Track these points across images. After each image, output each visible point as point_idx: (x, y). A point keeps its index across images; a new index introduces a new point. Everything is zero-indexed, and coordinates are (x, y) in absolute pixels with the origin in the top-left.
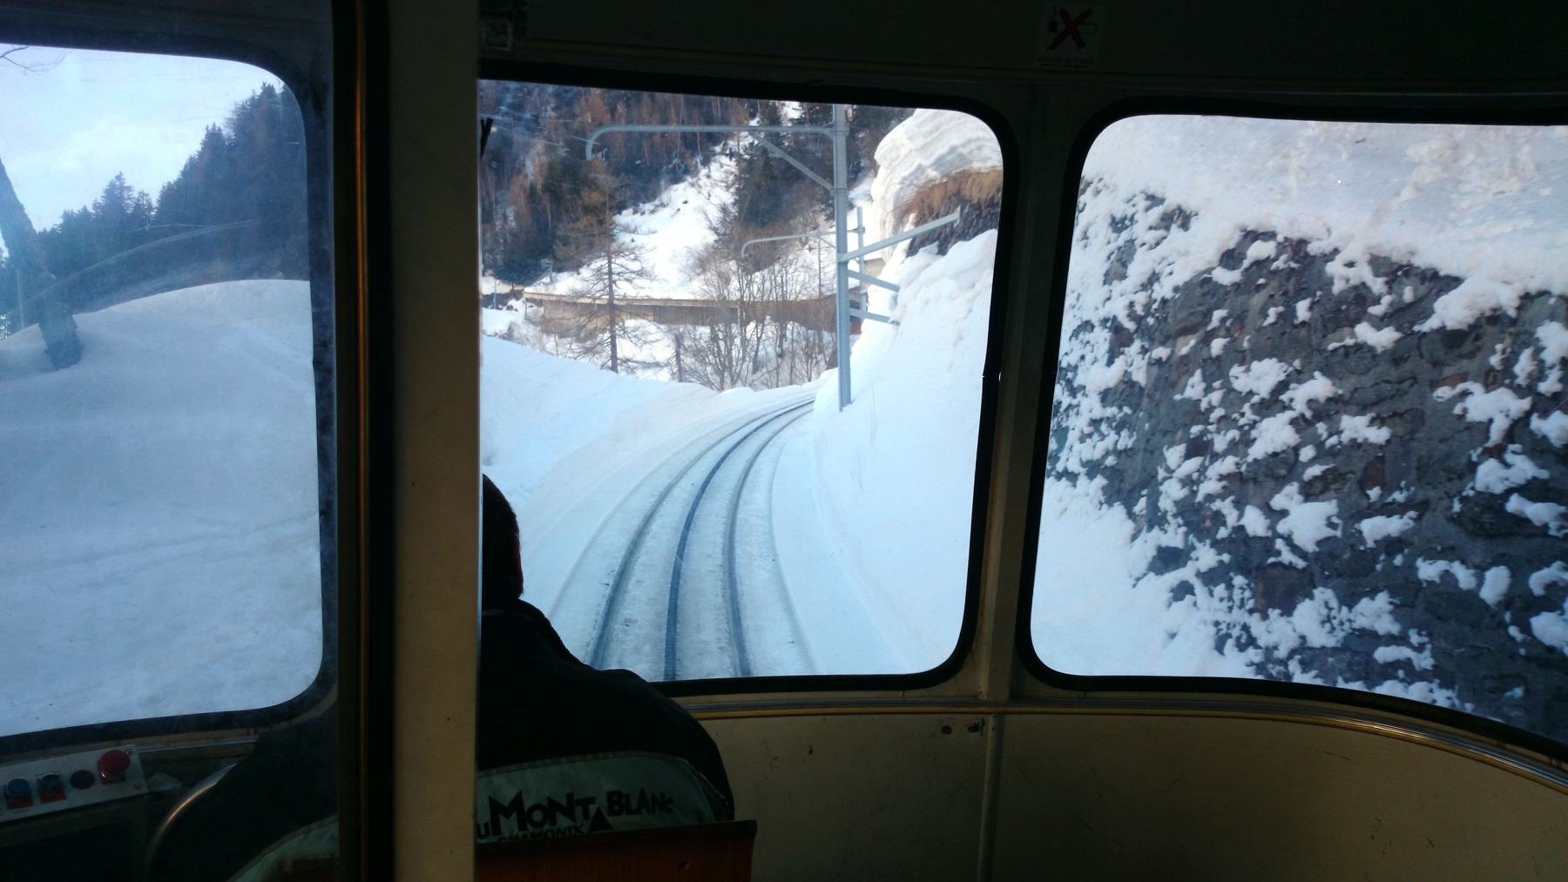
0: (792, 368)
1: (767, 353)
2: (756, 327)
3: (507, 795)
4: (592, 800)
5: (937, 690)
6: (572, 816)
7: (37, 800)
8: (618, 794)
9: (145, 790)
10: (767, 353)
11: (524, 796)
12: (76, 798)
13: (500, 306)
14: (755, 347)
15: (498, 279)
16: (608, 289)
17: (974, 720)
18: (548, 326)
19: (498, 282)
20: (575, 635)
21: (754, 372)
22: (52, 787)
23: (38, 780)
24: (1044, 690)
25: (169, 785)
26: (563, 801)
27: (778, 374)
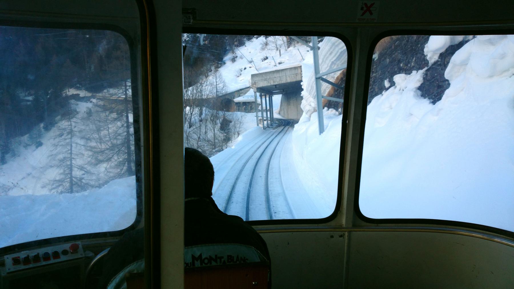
0: (206, 126)
1: (195, 120)
2: (190, 109)
3: (197, 254)
4: (223, 257)
5: (329, 224)
6: (216, 262)
7: (52, 258)
8: (231, 256)
9: (84, 256)
10: (195, 120)
11: (202, 255)
12: (63, 258)
13: (87, 101)
14: (190, 117)
15: (87, 91)
16: (124, 92)
17: (340, 233)
18: (105, 109)
19: (86, 92)
20: (221, 206)
21: (190, 128)
22: (56, 255)
23: (52, 252)
24: (364, 223)
25: (91, 254)
26: (214, 257)
27: (200, 128)
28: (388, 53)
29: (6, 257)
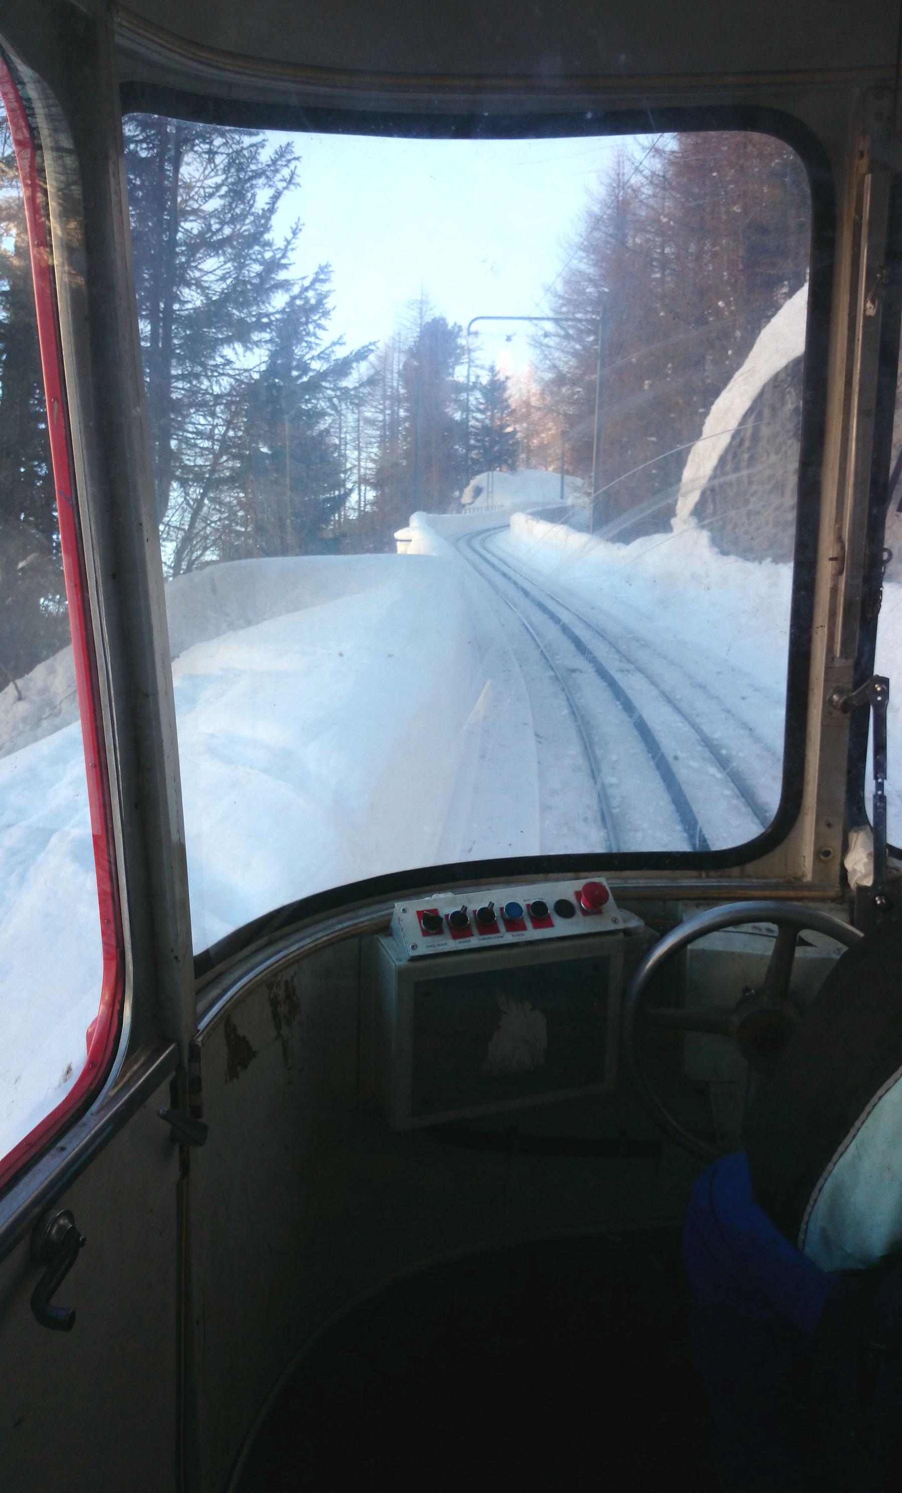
12: (562, 927)
28: (332, 386)
29: (399, 906)
